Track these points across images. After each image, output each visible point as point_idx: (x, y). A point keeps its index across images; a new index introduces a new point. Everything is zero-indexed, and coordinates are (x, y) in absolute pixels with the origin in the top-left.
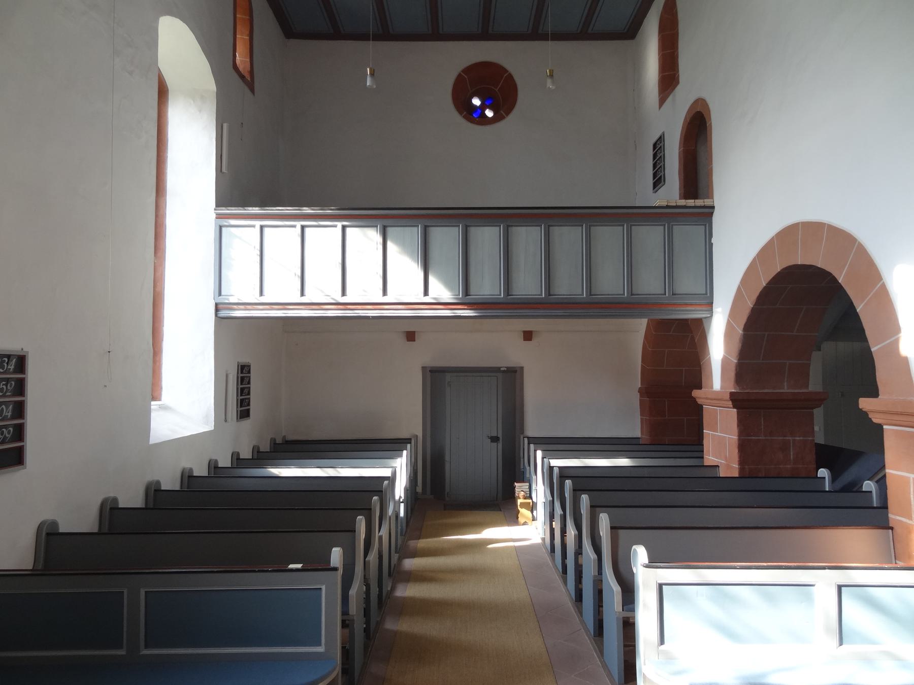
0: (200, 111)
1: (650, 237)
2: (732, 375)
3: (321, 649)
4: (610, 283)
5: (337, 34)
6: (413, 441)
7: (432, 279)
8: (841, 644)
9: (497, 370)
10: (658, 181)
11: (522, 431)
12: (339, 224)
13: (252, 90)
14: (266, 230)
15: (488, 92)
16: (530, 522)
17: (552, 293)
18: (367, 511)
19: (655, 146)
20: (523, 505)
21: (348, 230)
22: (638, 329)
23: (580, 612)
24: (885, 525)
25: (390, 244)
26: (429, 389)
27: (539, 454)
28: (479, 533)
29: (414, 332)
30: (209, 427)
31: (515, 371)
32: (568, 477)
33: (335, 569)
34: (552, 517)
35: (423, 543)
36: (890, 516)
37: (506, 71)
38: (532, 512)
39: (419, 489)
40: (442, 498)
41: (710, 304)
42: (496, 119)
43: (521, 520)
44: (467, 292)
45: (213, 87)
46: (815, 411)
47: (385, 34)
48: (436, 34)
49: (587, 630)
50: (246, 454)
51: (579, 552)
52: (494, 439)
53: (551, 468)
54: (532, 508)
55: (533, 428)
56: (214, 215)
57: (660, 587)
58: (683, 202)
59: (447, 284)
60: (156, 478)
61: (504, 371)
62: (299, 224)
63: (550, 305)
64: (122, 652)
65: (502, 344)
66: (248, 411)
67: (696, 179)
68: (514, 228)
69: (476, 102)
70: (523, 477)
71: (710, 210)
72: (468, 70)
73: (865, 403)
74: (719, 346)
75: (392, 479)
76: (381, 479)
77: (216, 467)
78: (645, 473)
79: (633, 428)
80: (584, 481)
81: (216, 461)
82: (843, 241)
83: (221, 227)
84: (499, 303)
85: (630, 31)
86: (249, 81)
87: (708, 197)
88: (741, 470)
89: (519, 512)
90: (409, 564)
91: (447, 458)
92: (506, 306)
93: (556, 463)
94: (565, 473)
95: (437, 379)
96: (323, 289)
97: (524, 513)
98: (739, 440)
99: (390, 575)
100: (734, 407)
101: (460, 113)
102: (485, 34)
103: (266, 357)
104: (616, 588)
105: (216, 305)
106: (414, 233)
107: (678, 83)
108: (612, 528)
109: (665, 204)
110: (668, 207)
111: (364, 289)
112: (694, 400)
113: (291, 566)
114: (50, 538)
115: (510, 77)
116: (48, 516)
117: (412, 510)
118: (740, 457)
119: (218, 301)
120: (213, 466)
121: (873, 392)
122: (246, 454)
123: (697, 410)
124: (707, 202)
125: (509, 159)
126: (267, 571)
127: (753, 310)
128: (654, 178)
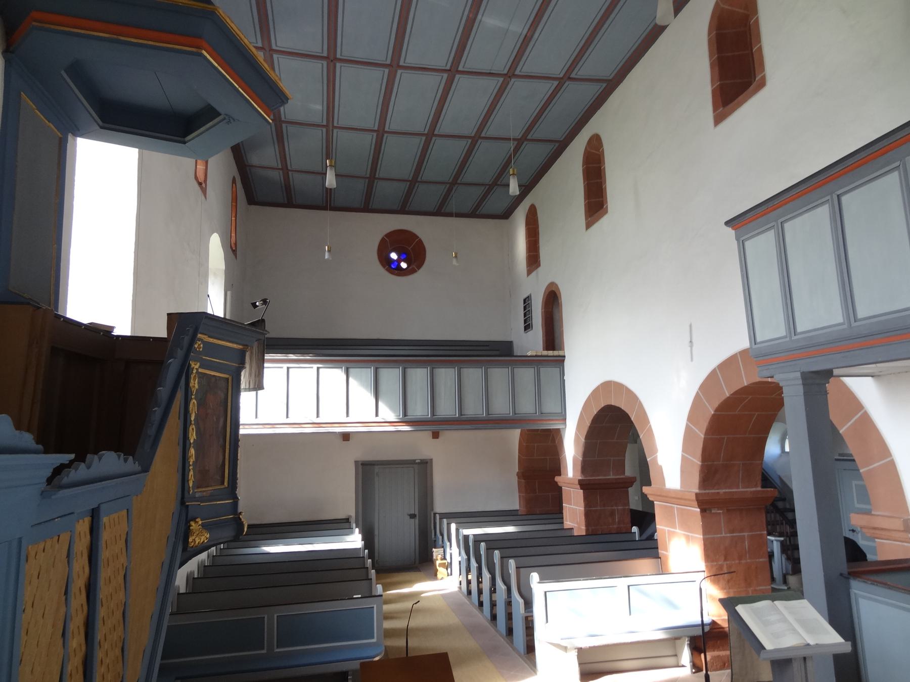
1: (526, 375)
2: (579, 468)
3: (374, 640)
4: (501, 407)
9: (413, 462)
10: (528, 327)
12: (315, 366)
15: (406, 252)
19: (525, 301)
20: (441, 565)
21: (321, 370)
22: (515, 435)
24: (657, 557)
25: (351, 379)
27: (453, 526)
34: (468, 571)
41: (565, 419)
43: (439, 576)
44: (405, 414)
45: (224, 267)
46: (630, 489)
49: (501, 635)
52: (412, 516)
53: (466, 538)
55: (441, 505)
58: (545, 353)
59: (392, 408)
62: (285, 366)
63: (462, 422)
64: (264, 651)
65: (425, 446)
67: (552, 338)
69: (394, 256)
73: (646, 490)
78: (527, 535)
79: (514, 503)
80: (493, 542)
85: (507, 214)
88: (587, 530)
91: (376, 533)
92: (435, 425)
93: (466, 532)
94: (478, 539)
95: (369, 472)
97: (442, 572)
101: (384, 266)
102: (403, 210)
104: (521, 601)
106: (369, 373)
109: (534, 354)
110: (536, 356)
115: (420, 242)
121: (648, 483)
124: (561, 353)
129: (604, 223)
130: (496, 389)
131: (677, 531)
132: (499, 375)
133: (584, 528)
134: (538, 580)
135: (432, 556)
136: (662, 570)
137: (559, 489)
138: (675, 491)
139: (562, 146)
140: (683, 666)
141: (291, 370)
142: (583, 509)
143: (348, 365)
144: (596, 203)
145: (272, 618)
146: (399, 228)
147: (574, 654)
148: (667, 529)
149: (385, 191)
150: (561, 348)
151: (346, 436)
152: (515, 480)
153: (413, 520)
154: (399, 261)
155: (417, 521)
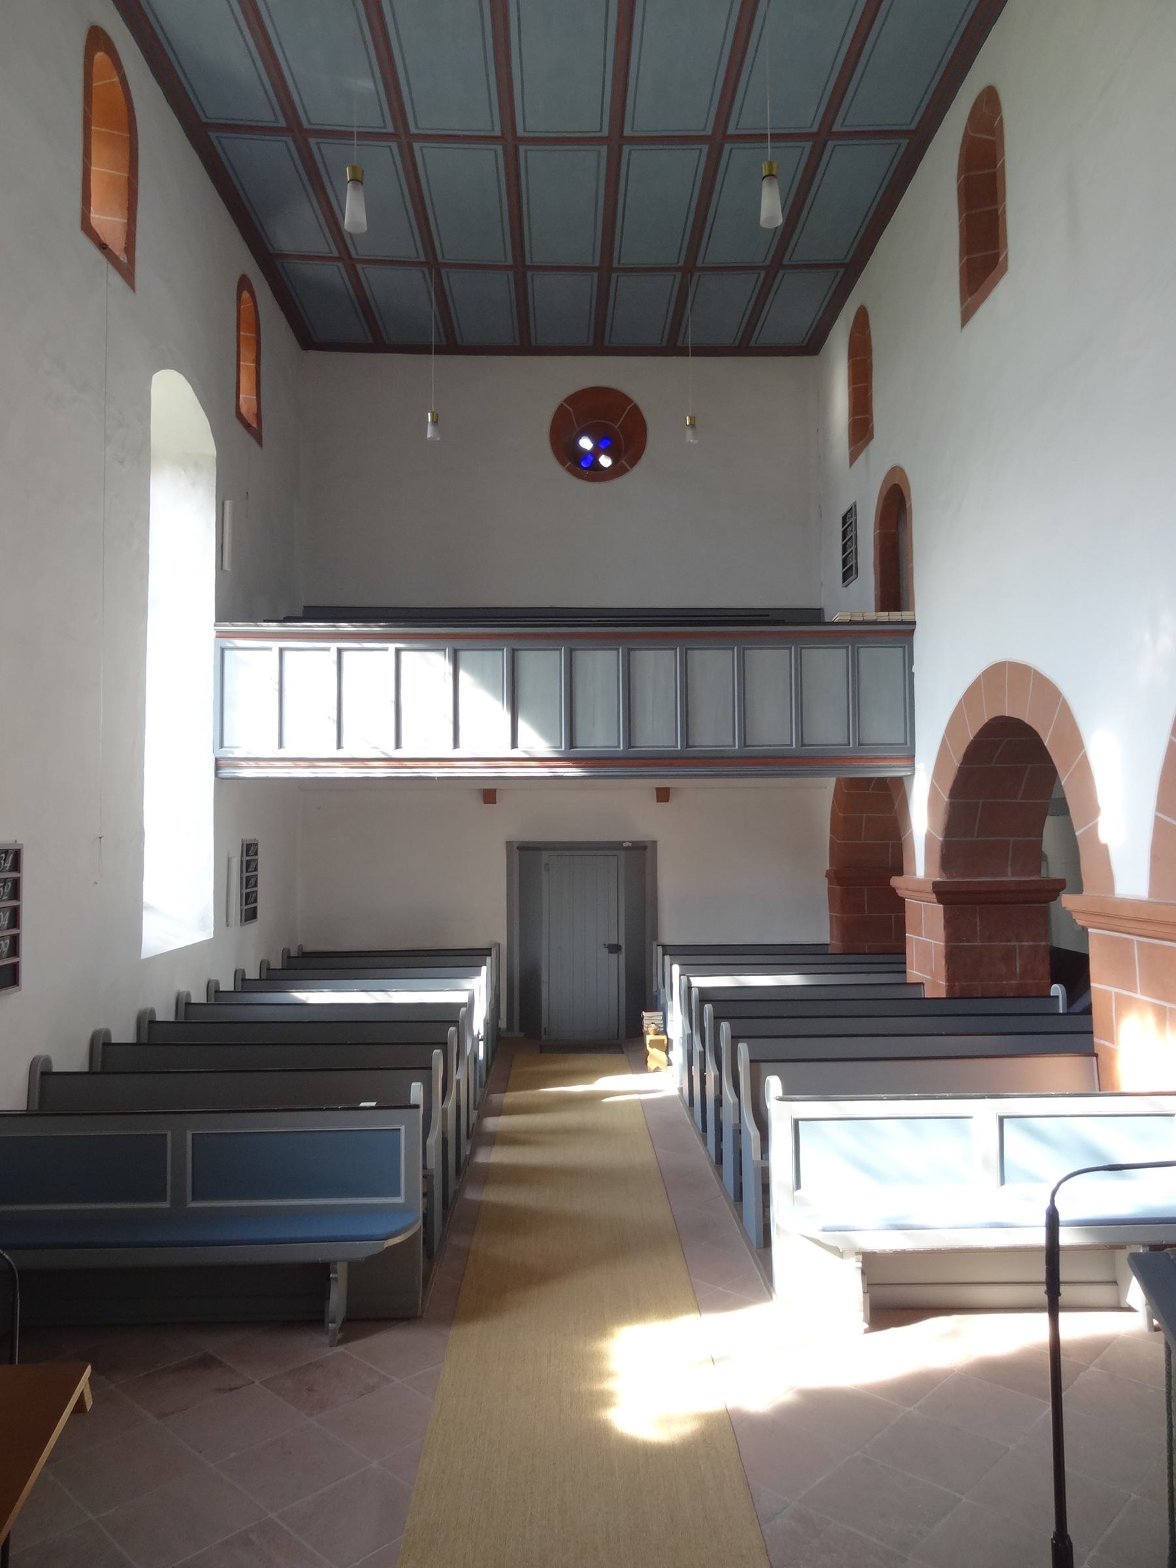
0: (194, 485)
1: (827, 664)
2: (937, 857)
3: (400, 1200)
4: (772, 729)
5: (378, 344)
6: (494, 952)
7: (522, 724)
8: (1003, 1182)
9: (617, 846)
10: (849, 572)
11: (655, 937)
12: (392, 647)
13: (259, 440)
14: (287, 654)
15: (605, 431)
16: (663, 1067)
17: (690, 743)
18: (444, 1045)
19: (844, 519)
20: (654, 1044)
21: (404, 654)
23: (720, 1176)
24: (1090, 1052)
25: (463, 675)
26: (516, 881)
27: (676, 969)
28: (591, 1083)
29: (495, 790)
30: (207, 934)
31: (645, 848)
32: (708, 1001)
33: (417, 1107)
35: (510, 1098)
36: (1095, 1040)
37: (628, 400)
38: (667, 1053)
39: (503, 1024)
40: (534, 1035)
41: (912, 758)
42: (617, 471)
43: (651, 1064)
44: (571, 743)
45: (214, 452)
47: (451, 345)
48: (525, 345)
50: (252, 973)
51: (719, 1102)
52: (614, 949)
54: (667, 1047)
55: (671, 931)
56: (214, 634)
57: (796, 1123)
59: (544, 732)
60: (149, 1006)
61: (627, 848)
62: (334, 646)
63: (690, 760)
64: (166, 1205)
65: (629, 810)
66: (255, 909)
67: (894, 589)
68: (637, 652)
69: (586, 443)
70: (655, 1003)
71: (910, 627)
72: (573, 399)
74: (922, 819)
75: (470, 1006)
76: (456, 1007)
77: (217, 991)
78: (822, 994)
79: (819, 930)
80: (726, 1005)
81: (217, 983)
82: (1047, 692)
83: (223, 650)
84: (618, 759)
85: (812, 345)
86: (254, 429)
87: (908, 610)
88: (950, 988)
89: (648, 1053)
90: (492, 1123)
91: (544, 977)
93: (699, 982)
94: (706, 995)
95: (528, 859)
96: (369, 741)
97: (656, 1056)
98: (947, 947)
99: (468, 1137)
100: (939, 902)
101: (563, 463)
102: (598, 345)
103: (279, 831)
105: (217, 760)
106: (497, 660)
107: (871, 437)
108: (751, 1061)
109: (847, 618)
111: (426, 739)
112: (893, 891)
113: (362, 1104)
114: (44, 1077)
116: (40, 1051)
117: (494, 1052)
118: (948, 970)
119: (219, 756)
120: (213, 989)
122: (252, 973)
123: (899, 904)
124: (905, 615)
125: (633, 539)
126: (337, 1109)
127: (960, 770)
128: (844, 566)
129: (1002, 296)
130: (770, 694)
131: (1138, 996)
132: (770, 663)
133: (943, 983)
134: (780, 1094)
135: (642, 1027)
136: (1100, 1083)
137: (900, 903)
138: (1136, 904)
139: (916, 143)
140: (1130, 1309)
141: (345, 654)
142: (942, 943)
143: (458, 644)
144: (983, 256)
145: (182, 1136)
146: (592, 384)
147: (852, 1269)
148: (1114, 990)
149: (561, 299)
150: (910, 607)
151: (489, 793)
152: (821, 888)
153: (614, 957)
154: (595, 454)
155: (622, 957)
